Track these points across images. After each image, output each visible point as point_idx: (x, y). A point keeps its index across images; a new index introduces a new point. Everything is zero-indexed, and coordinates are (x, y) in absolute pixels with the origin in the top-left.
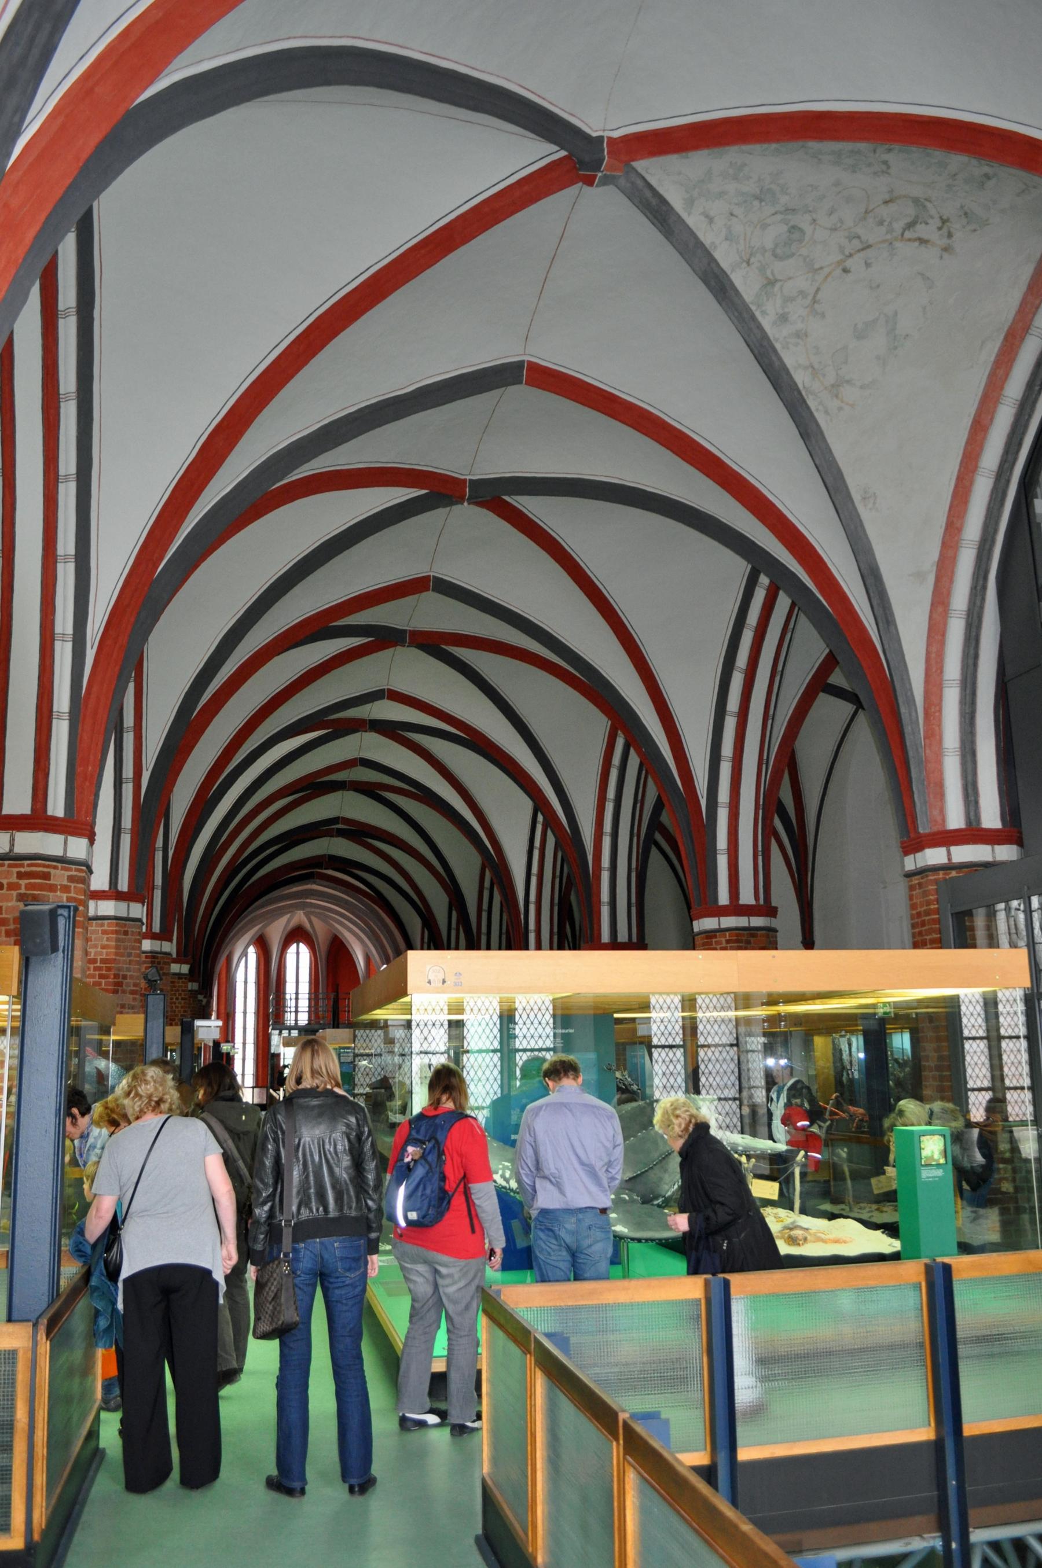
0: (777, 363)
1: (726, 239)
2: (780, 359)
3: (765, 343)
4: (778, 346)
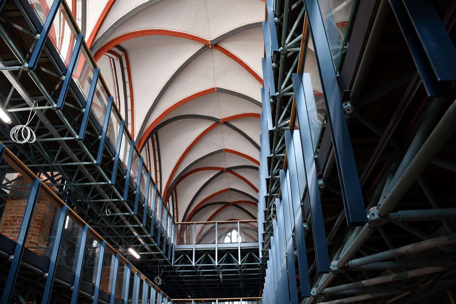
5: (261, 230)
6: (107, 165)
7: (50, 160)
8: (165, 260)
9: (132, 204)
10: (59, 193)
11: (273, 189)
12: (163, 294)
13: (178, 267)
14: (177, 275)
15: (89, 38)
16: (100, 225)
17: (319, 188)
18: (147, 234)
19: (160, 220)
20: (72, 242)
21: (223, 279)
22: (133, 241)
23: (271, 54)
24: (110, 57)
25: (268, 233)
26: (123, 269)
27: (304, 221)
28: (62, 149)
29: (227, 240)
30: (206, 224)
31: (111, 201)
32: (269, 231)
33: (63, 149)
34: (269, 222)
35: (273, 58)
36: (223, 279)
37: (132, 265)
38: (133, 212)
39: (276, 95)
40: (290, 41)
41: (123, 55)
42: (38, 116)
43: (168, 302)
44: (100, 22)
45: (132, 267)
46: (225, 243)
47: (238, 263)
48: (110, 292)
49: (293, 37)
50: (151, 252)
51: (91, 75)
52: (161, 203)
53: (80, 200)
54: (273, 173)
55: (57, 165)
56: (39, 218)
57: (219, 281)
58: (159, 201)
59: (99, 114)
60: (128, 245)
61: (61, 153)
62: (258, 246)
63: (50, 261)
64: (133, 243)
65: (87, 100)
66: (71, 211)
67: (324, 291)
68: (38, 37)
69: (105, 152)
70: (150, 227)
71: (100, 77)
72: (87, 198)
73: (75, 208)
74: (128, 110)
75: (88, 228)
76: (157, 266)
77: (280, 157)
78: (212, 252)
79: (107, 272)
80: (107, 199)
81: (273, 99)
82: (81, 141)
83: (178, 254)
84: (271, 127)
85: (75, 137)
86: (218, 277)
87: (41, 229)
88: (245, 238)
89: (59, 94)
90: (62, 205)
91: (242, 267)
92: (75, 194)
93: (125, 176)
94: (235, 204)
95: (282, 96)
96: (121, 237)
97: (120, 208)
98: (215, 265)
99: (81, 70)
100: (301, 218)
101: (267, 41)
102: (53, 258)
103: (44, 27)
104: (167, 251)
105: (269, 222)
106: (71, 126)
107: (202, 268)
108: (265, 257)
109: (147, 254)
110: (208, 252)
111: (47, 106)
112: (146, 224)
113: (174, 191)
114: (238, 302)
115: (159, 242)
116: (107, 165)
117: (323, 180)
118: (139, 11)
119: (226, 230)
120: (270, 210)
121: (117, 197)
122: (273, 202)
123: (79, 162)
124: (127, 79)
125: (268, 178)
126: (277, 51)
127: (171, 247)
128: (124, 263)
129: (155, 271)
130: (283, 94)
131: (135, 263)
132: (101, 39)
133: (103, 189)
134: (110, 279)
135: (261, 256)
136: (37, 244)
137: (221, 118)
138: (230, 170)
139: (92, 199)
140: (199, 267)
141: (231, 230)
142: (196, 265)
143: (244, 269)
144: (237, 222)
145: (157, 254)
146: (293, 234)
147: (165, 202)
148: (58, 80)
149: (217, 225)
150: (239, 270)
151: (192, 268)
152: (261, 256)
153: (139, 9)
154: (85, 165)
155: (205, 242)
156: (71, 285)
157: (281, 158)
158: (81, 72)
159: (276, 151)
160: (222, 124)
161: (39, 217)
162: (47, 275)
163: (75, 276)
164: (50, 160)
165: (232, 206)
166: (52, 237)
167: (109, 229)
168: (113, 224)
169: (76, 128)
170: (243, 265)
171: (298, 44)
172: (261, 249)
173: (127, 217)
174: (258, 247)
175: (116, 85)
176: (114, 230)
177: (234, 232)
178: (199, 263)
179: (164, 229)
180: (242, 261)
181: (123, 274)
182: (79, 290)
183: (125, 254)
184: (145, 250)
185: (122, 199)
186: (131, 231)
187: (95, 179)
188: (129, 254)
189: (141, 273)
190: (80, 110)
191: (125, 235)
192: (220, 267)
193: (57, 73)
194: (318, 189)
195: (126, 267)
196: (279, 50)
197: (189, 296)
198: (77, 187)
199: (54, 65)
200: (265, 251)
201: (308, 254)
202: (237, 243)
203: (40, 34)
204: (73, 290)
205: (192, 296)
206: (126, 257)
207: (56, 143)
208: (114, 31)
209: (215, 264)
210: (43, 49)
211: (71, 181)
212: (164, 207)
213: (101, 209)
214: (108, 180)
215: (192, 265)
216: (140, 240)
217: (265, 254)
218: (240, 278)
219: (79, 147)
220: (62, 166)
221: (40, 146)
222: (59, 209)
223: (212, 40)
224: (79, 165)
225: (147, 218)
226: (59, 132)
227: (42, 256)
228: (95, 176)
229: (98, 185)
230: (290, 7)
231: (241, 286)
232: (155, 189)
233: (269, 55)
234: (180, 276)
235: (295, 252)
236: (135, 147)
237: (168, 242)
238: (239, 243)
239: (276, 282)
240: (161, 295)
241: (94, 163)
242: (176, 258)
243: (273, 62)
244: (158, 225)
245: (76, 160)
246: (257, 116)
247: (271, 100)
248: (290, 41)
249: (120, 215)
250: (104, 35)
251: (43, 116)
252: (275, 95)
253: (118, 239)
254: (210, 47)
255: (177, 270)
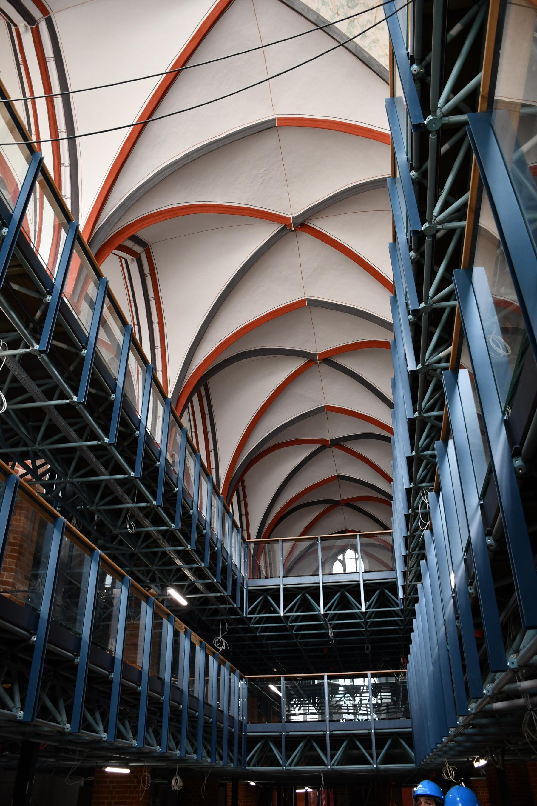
0: (367, 56)
1: (323, 5)
2: (368, 54)
3: (358, 48)
4: (366, 49)
5: (400, 550)
6: (126, 444)
7: (31, 440)
8: (231, 606)
9: (172, 511)
10: (46, 496)
11: (420, 473)
12: (230, 667)
13: (253, 619)
14: (252, 632)
15: (85, 227)
16: (118, 549)
17: (516, 473)
18: (198, 561)
19: (219, 537)
20: (70, 579)
21: (335, 639)
22: (174, 576)
23: (405, 236)
24: (120, 257)
25: (413, 554)
26: (161, 624)
27: (488, 534)
28: (50, 420)
29: (337, 568)
30: (299, 542)
31: (135, 507)
32: (414, 551)
33: (51, 420)
34: (415, 533)
35: (411, 243)
36: (335, 639)
37: (176, 618)
38: (174, 524)
39: (420, 307)
40: (442, 210)
41: (142, 252)
42: (8, 366)
43: (239, 682)
44: (102, 199)
45: (176, 621)
46: (333, 573)
47: (361, 610)
48: (141, 665)
49: (446, 205)
50: (206, 593)
51: (92, 290)
52: (221, 506)
53: (83, 507)
54: (420, 446)
55: (43, 447)
56: (14, 541)
57: (326, 641)
58: (216, 502)
59: (107, 356)
60: (165, 583)
61: (48, 427)
62: (395, 577)
63: (39, 614)
64: (175, 578)
65: (89, 334)
66: (71, 527)
67: (531, 660)
68: (5, 233)
69: (123, 422)
70: (204, 549)
71: (108, 293)
72: (95, 504)
73: (74, 521)
74: (156, 347)
75: (100, 555)
76: (219, 618)
77: (430, 417)
78: (314, 591)
79: (131, 629)
80: (128, 503)
81: (413, 316)
82: (81, 406)
83: (253, 595)
84: (412, 366)
85: (72, 398)
86: (327, 635)
87: (18, 559)
88: (369, 562)
89: (42, 327)
90: (55, 518)
91: (367, 616)
92: (74, 496)
93: (158, 463)
94: (349, 504)
95: (430, 310)
96: (154, 568)
97: (150, 517)
98: (319, 613)
99: (74, 282)
100: (481, 527)
101: (398, 213)
102: (44, 609)
103: (14, 216)
104: (234, 590)
105: (415, 533)
106: (63, 380)
107: (296, 619)
108: (409, 596)
109: (200, 598)
110: (307, 590)
111: (23, 348)
112: (197, 546)
113: (240, 484)
114: (362, 679)
115: (220, 575)
116: (126, 444)
117: (522, 460)
118: (167, 174)
119: (334, 551)
120: (415, 512)
121: (146, 500)
122: (421, 497)
123: (79, 442)
124: (151, 294)
125: (410, 456)
126: (419, 230)
127: (241, 583)
128: (162, 615)
129: (214, 627)
130: (432, 305)
131: (178, 613)
132: (106, 227)
133: (121, 487)
134: (140, 643)
135: (401, 595)
136: (13, 585)
137: (317, 353)
138: (338, 443)
139: (102, 505)
140: (291, 617)
141: (343, 550)
142: (285, 615)
143: (371, 620)
144: (356, 535)
145: (216, 597)
146: (465, 557)
147: (226, 502)
148: (39, 302)
149: (320, 541)
150: (363, 620)
151: (278, 619)
152: (401, 595)
153: (168, 172)
154: (89, 447)
155: (301, 574)
156: (75, 655)
157: (432, 418)
158: (73, 287)
159: (423, 407)
160: (320, 363)
161: (14, 538)
162: (36, 639)
163: (80, 639)
164: (31, 440)
165: (344, 507)
166: (40, 572)
167: (132, 555)
168: (139, 547)
169: (72, 383)
170: (370, 611)
171: (460, 214)
172: (400, 583)
173: (164, 534)
174: (395, 578)
175: (133, 305)
176: (142, 558)
177: (350, 553)
178: (290, 611)
179: (227, 552)
180: (367, 606)
181: (161, 633)
182: (88, 663)
183: (161, 599)
184: (195, 590)
185: (155, 503)
186: (171, 558)
187: (106, 469)
188: (167, 598)
189: (192, 631)
190: (77, 351)
191: (160, 566)
192: (328, 618)
193: (38, 291)
194: (514, 476)
195: (165, 621)
196: (423, 229)
197: (275, 670)
198: (76, 484)
199: (33, 280)
200: (409, 586)
201: (498, 592)
202: (356, 573)
203: (8, 228)
204: (78, 665)
205: (280, 670)
206: (162, 602)
207: (40, 412)
208: (125, 212)
209: (320, 612)
210: (13, 252)
211: (66, 475)
212: (226, 514)
213: (118, 522)
214: (130, 470)
215: (279, 615)
216: (187, 573)
217: (408, 591)
218: (364, 636)
219: (79, 415)
220: (50, 450)
221: (11, 416)
222: (50, 525)
223: (295, 216)
224: (80, 447)
225: (198, 533)
226: (44, 392)
227: (20, 604)
228: (106, 465)
229: (113, 480)
230: (438, 150)
231: (368, 649)
232: (210, 482)
233: (403, 237)
234: (258, 634)
235: (471, 589)
236: (172, 412)
237: (236, 575)
238: (361, 573)
239: (435, 642)
240: (227, 669)
241: (105, 441)
242: (250, 602)
243: (410, 250)
244: (216, 547)
245: (74, 439)
246: (385, 345)
247: (410, 317)
248: (442, 210)
249: (152, 531)
250: (109, 220)
251: (16, 365)
252: (417, 308)
253: (148, 572)
254: (293, 229)
255: (253, 625)
